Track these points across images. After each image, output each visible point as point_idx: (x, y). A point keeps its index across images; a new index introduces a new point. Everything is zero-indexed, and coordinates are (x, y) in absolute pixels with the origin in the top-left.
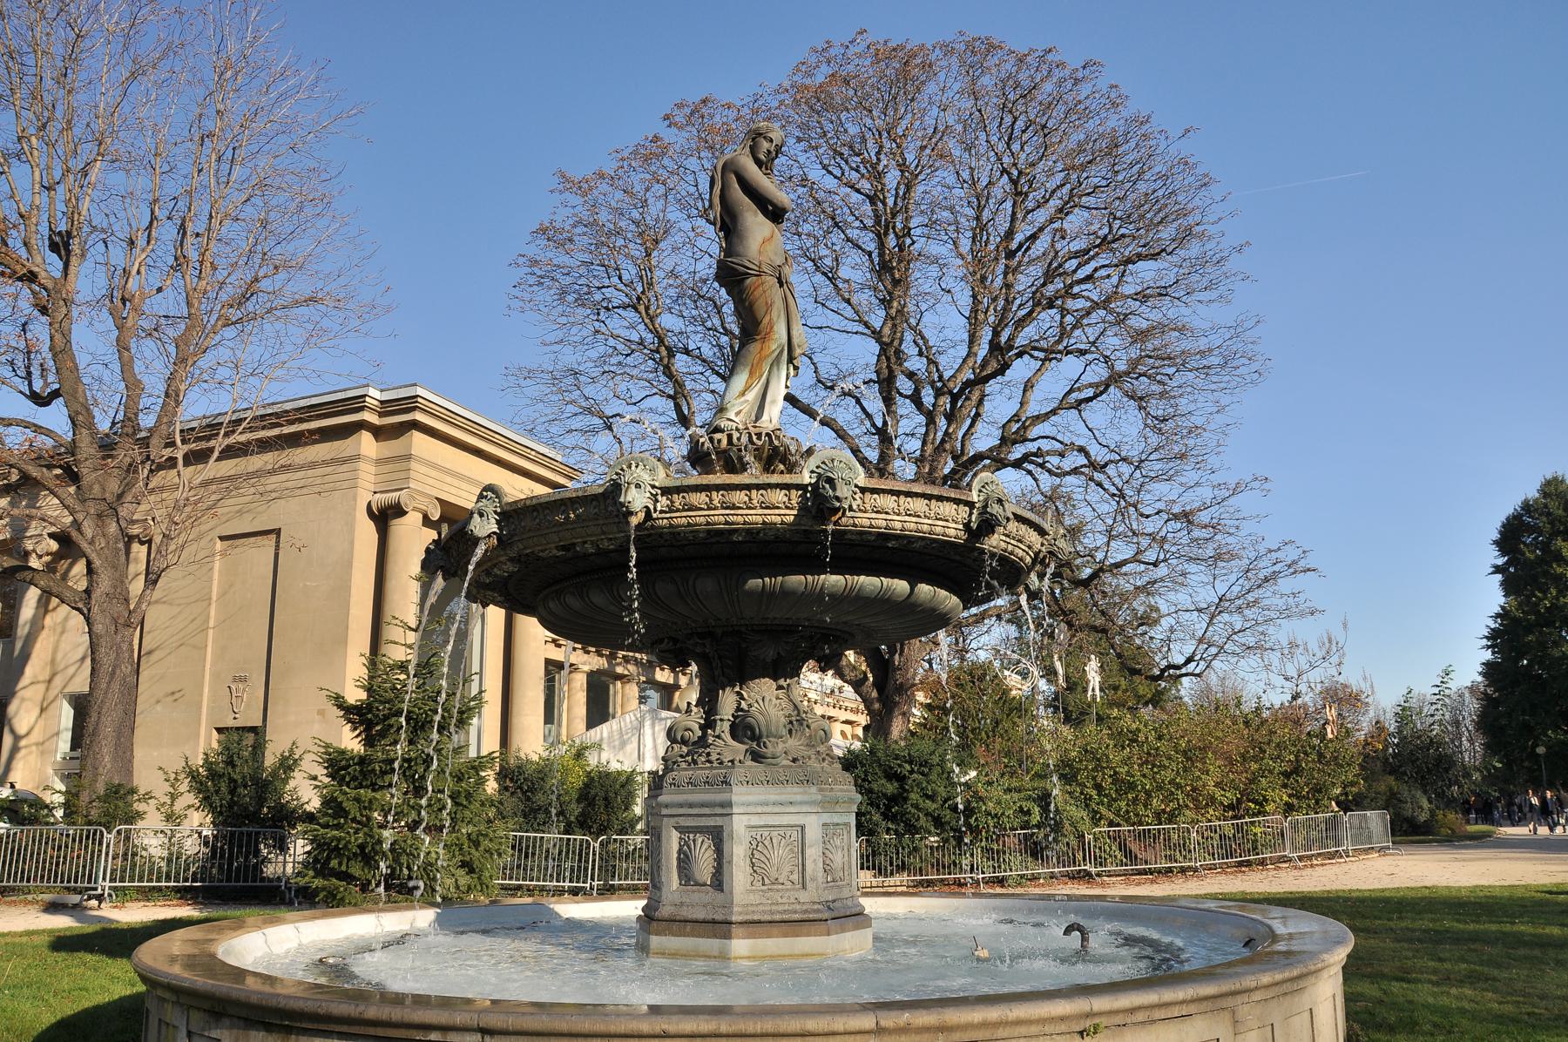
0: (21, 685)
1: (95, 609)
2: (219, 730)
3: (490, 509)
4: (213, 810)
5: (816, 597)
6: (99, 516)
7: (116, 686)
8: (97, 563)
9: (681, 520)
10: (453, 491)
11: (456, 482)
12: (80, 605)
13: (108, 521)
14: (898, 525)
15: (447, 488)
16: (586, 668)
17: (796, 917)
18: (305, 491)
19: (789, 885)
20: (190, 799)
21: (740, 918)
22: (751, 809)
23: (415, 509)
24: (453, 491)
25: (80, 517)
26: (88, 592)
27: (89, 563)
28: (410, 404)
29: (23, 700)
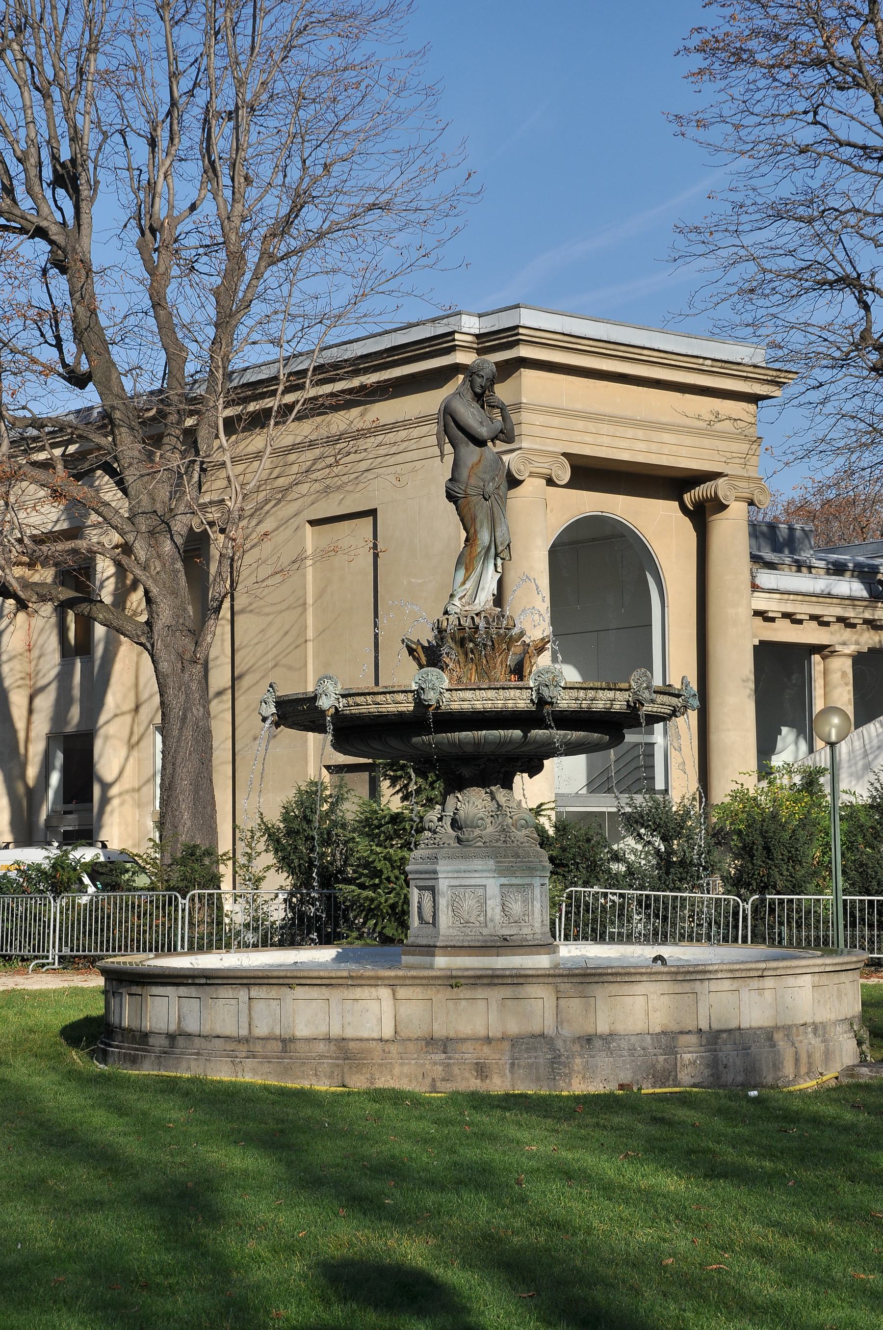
0: (103, 719)
1: (159, 645)
2: (328, 767)
3: (270, 700)
4: (292, 871)
5: (461, 743)
6: (152, 533)
7: (188, 733)
8: (155, 591)
9: (355, 710)
10: (588, 438)
11: (591, 426)
12: (143, 640)
13: (162, 538)
14: (479, 706)
15: (578, 437)
16: (851, 649)
17: (478, 944)
18: (399, 458)
19: (478, 924)
20: (269, 858)
21: (442, 944)
22: (450, 875)
23: (532, 475)
24: (588, 438)
25: (130, 538)
26: (149, 623)
27: (147, 592)
28: (508, 337)
29: (107, 738)
